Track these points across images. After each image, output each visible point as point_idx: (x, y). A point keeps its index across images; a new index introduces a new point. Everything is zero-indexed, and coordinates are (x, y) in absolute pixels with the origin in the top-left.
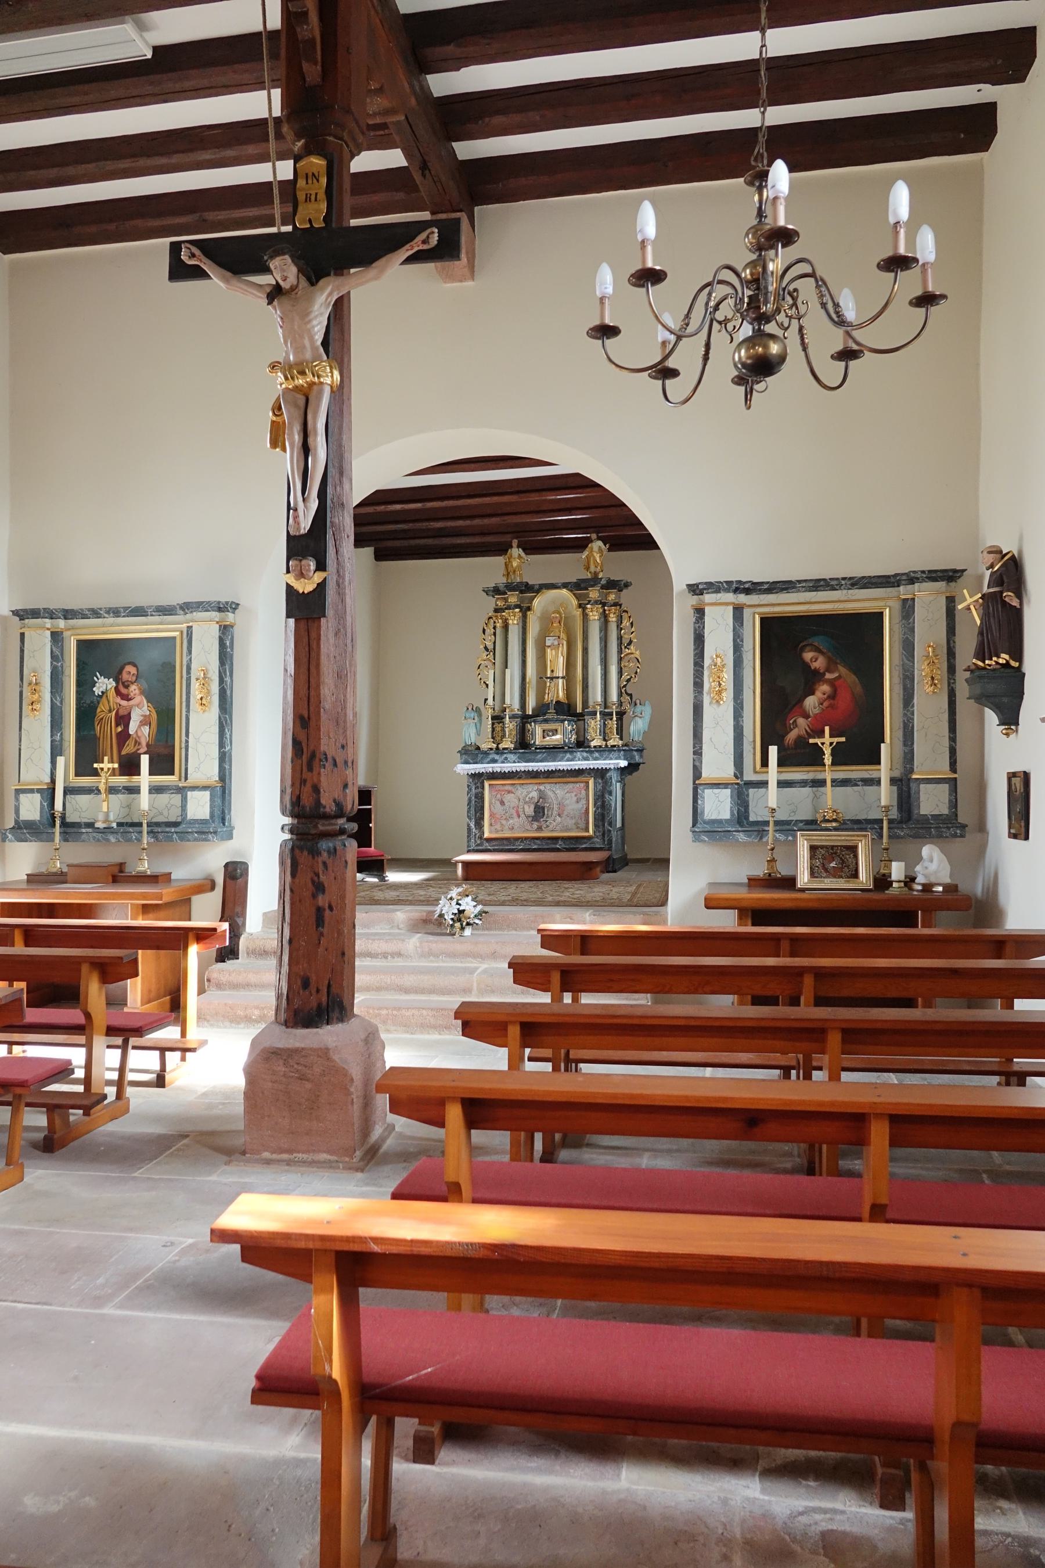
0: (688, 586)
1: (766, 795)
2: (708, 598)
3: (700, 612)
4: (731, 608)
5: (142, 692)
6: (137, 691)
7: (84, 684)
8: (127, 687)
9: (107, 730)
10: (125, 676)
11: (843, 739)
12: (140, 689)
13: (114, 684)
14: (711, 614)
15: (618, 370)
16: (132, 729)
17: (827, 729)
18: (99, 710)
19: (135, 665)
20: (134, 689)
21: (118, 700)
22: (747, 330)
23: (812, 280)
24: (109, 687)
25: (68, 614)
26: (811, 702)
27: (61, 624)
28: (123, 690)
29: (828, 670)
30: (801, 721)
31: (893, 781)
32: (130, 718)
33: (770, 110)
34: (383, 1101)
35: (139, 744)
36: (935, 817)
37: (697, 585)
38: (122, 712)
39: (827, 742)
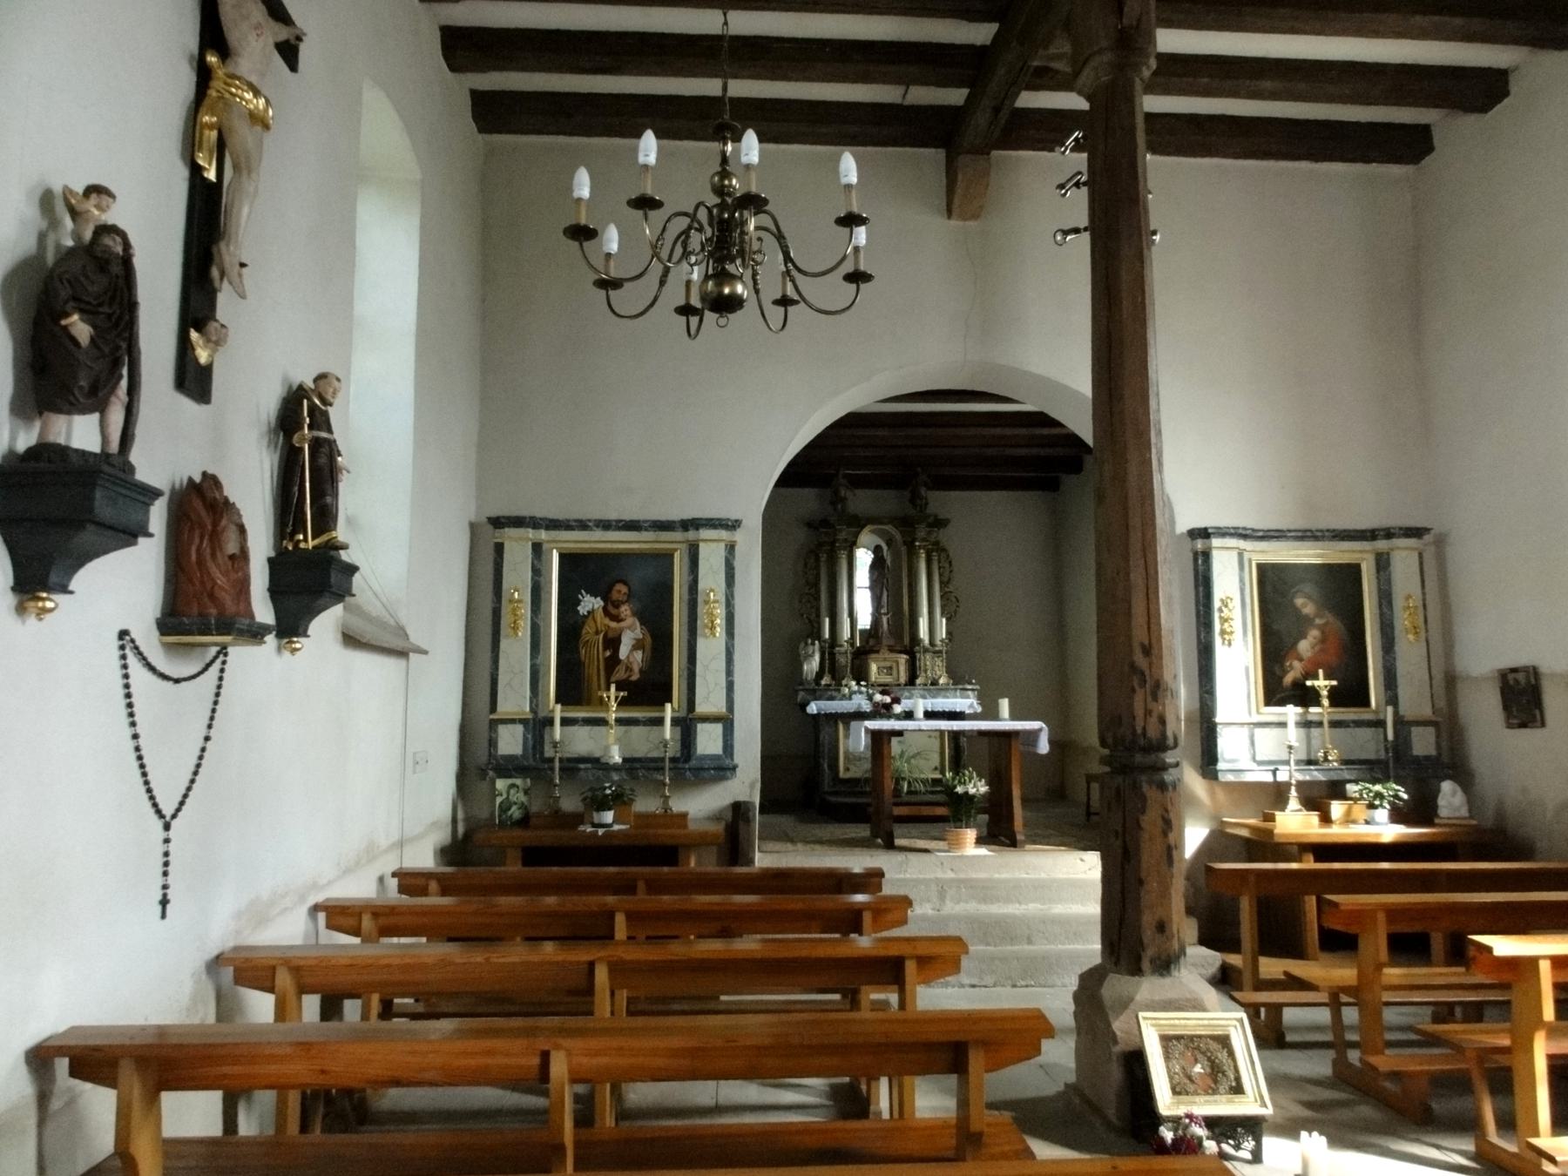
1: (663, 732)
2: (1216, 542)
3: (499, 549)
4: (722, 545)
5: (634, 614)
8: (617, 607)
9: (593, 654)
10: (615, 596)
11: (1334, 683)
14: (704, 551)
15: (837, 317)
16: (624, 652)
17: (1321, 672)
19: (625, 583)
20: (625, 610)
21: (607, 621)
25: (553, 525)
26: (1304, 647)
27: (543, 535)
28: (613, 611)
29: (1317, 615)
30: (1296, 664)
31: (675, 722)
34: (62, 1065)
36: (1427, 758)
38: (611, 635)
39: (1322, 683)
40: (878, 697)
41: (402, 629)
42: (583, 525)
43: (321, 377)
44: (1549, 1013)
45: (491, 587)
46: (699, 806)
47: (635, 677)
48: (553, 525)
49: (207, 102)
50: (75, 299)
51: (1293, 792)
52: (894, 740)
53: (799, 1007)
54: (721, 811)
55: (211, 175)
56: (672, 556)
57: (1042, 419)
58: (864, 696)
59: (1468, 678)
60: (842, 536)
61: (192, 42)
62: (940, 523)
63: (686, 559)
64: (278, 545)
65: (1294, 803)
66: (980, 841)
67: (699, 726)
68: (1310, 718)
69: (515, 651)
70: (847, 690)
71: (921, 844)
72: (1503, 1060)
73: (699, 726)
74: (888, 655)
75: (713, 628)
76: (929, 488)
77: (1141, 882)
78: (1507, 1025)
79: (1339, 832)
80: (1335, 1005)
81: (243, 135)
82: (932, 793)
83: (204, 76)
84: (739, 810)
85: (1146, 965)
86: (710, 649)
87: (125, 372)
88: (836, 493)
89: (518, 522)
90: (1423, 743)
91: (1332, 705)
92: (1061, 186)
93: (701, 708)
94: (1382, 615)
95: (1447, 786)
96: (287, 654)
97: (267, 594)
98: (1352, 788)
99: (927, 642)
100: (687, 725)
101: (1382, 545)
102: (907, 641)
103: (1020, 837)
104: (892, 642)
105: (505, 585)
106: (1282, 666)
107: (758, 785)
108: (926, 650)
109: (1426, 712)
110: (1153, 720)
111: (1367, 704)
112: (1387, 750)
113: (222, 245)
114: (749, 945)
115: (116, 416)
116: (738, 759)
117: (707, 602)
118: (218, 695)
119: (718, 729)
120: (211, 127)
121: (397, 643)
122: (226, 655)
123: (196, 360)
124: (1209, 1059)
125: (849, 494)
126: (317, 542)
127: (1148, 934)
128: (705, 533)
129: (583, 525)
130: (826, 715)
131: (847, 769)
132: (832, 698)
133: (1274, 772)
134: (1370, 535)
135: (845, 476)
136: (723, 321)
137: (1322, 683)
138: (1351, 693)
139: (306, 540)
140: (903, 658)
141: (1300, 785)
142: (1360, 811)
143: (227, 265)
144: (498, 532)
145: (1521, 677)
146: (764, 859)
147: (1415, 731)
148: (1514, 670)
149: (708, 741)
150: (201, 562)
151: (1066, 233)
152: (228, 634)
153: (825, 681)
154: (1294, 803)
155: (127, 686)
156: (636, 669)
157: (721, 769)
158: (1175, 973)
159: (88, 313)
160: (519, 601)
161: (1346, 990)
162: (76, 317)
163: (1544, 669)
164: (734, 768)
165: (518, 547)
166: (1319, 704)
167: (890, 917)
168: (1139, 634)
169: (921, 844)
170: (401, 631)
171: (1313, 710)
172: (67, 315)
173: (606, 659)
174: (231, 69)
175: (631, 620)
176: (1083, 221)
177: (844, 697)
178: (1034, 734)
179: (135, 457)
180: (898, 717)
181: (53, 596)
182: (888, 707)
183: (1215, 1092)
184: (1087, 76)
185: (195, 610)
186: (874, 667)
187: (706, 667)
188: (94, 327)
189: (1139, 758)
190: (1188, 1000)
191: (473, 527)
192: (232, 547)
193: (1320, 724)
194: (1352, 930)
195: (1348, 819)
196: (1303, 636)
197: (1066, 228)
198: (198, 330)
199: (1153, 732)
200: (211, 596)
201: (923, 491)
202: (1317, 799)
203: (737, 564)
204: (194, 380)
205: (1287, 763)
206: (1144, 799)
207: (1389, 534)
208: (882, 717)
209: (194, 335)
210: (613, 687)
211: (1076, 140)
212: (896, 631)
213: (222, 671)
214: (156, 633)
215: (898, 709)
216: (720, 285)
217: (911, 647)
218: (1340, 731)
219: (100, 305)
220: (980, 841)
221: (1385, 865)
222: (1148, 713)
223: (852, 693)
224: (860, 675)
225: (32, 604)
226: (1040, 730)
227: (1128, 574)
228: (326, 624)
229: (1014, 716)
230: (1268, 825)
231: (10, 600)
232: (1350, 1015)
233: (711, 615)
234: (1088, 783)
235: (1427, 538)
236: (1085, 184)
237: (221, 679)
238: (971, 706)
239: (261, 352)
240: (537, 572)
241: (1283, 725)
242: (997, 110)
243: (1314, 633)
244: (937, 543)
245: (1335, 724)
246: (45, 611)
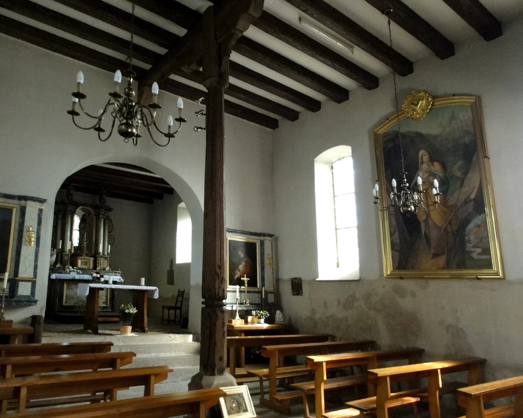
1: (3, 285)
30: (238, 273)
31: (9, 280)
39: (245, 279)
40: (95, 275)
44: (325, 378)
46: (17, 316)
51: (237, 314)
52: (100, 291)
53: (77, 400)
54: (27, 319)
57: (161, 181)
58: (76, 273)
59: (283, 280)
60: (70, 208)
62: (109, 209)
65: (238, 317)
66: (133, 331)
67: (20, 283)
68: (242, 290)
70: (68, 270)
71: (107, 332)
72: (312, 392)
73: (20, 283)
74: (86, 257)
76: (107, 196)
77: (215, 344)
78: (314, 382)
79: (249, 326)
80: (261, 381)
82: (103, 312)
84: (35, 319)
85: (216, 372)
86: (27, 252)
88: (68, 191)
90: (271, 299)
91: (248, 286)
92: (197, 113)
93: (22, 274)
94: (261, 259)
95: (278, 312)
98: (254, 313)
99: (101, 254)
100: (14, 283)
101: (262, 238)
102: (93, 252)
103: (146, 329)
104: (87, 252)
106: (234, 272)
107: (45, 309)
108: (101, 257)
109: (272, 289)
110: (221, 290)
111: (257, 286)
112: (262, 300)
114: (65, 375)
116: (36, 298)
119: (30, 284)
124: (237, 402)
125: (74, 193)
127: (217, 361)
130: (59, 279)
131: (67, 302)
132: (60, 273)
133: (232, 307)
134: (259, 235)
135: (73, 186)
136: (126, 140)
137: (245, 279)
138: (252, 283)
140: (92, 259)
141: (239, 311)
142: (256, 319)
145: (297, 281)
146: (46, 340)
147: (269, 295)
148: (295, 279)
149: (24, 289)
151: (198, 128)
153: (58, 265)
154: (238, 317)
157: (30, 301)
158: (224, 374)
161: (265, 376)
163: (303, 279)
164: (36, 301)
166: (244, 286)
167: (127, 360)
168: (218, 262)
169: (107, 332)
171: (242, 287)
176: (204, 126)
177: (66, 273)
178: (153, 292)
180: (103, 283)
182: (98, 279)
183: (239, 412)
184: (208, 82)
186: (79, 262)
189: (216, 302)
190: (229, 383)
193: (244, 292)
194: (269, 357)
195: (253, 322)
196: (241, 264)
197: (198, 126)
199: (221, 295)
201: (104, 196)
202: (244, 315)
203: (43, 217)
205: (236, 304)
206: (217, 316)
207: (264, 235)
208: (96, 282)
211: (202, 100)
212: (89, 248)
215: (102, 280)
217: (95, 255)
218: (249, 294)
220: (133, 331)
221: (263, 337)
222: (220, 287)
223: (70, 271)
224: (74, 264)
226: (156, 290)
227: (215, 242)
229: (146, 284)
230: (230, 324)
232: (266, 384)
233: (30, 237)
234: (163, 309)
235: (273, 238)
236: (205, 114)
238: (120, 279)
241: (235, 292)
242: (163, 77)
243: (243, 263)
244: (108, 217)
245: (248, 292)
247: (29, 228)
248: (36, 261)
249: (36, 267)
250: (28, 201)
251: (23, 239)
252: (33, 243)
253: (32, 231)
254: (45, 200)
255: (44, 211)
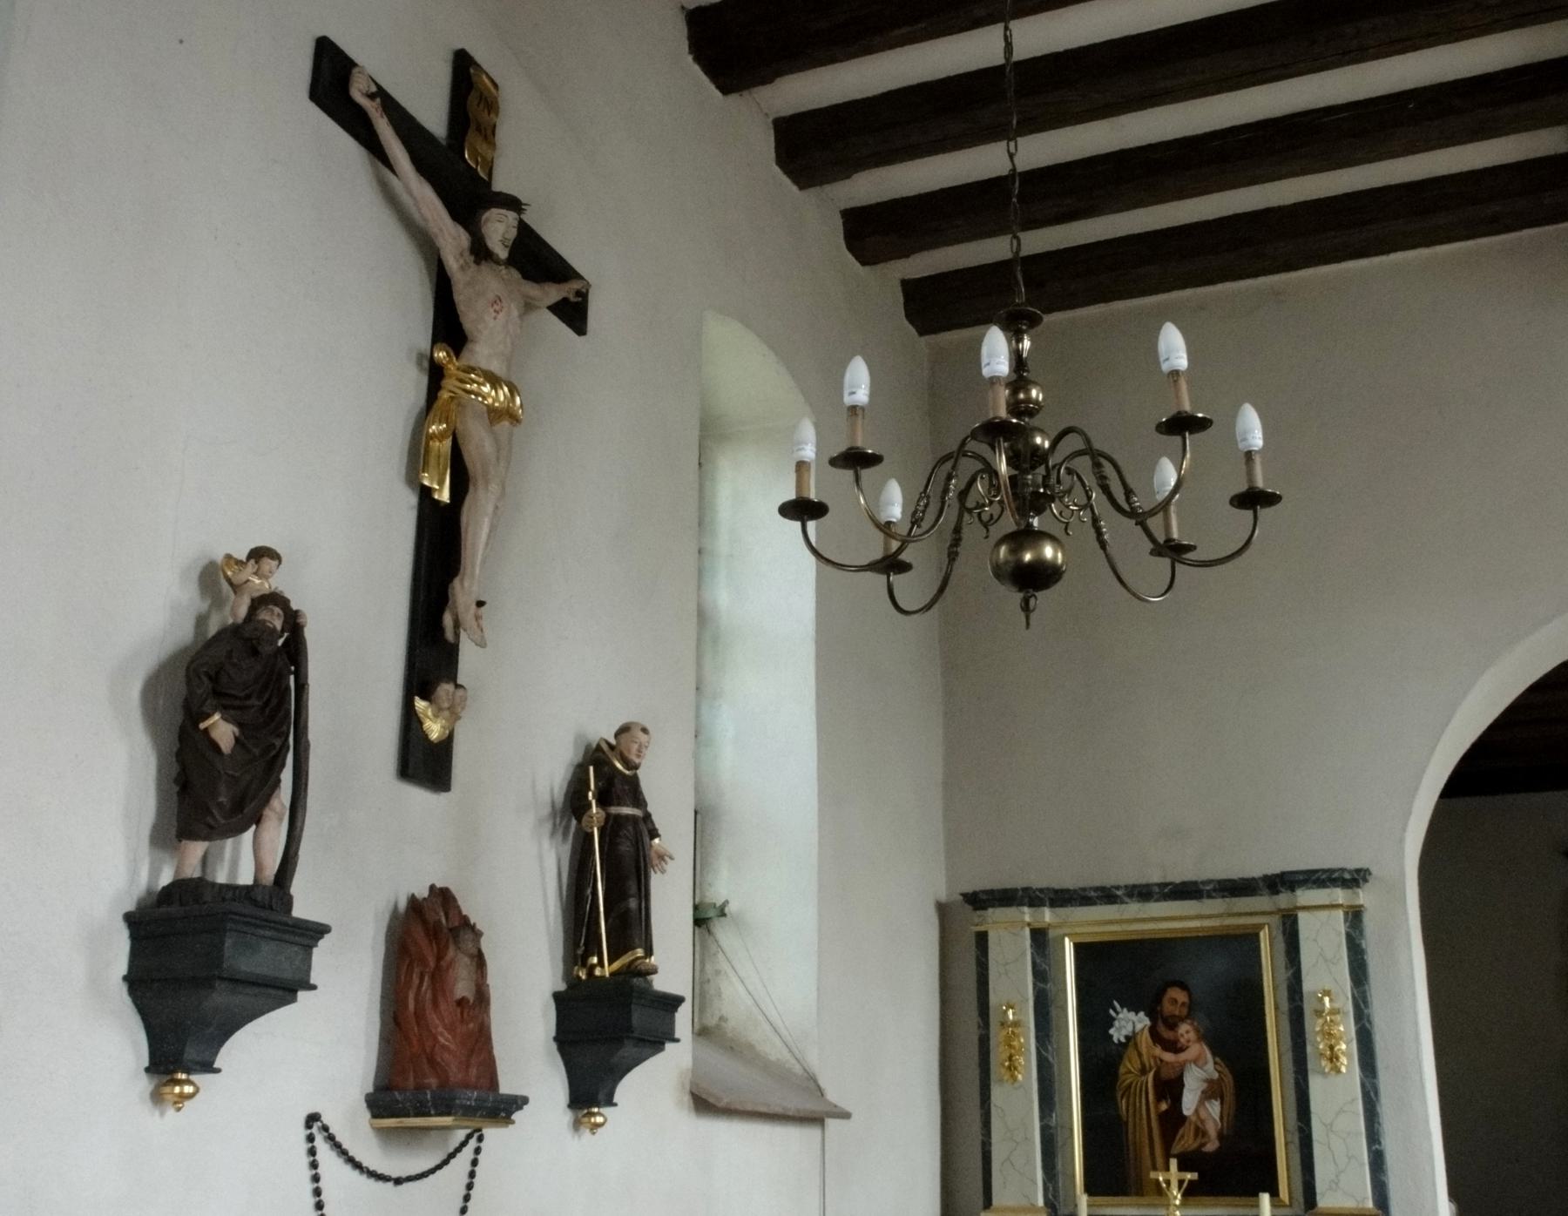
0: (964, 895)
3: (982, 939)
4: (1340, 914)
5: (1203, 1037)
6: (1192, 1035)
7: (1094, 1023)
8: (1173, 1026)
10: (1167, 1008)
12: (1197, 1031)
13: (1147, 1022)
14: (1307, 924)
18: (1122, 1070)
19: (1183, 986)
20: (1185, 1031)
21: (1158, 1051)
22: (1009, 524)
23: (1087, 458)
24: (1139, 1027)
25: (1061, 898)
27: (1047, 915)
28: (1167, 1034)
32: (1183, 1085)
33: (1024, 236)
35: (1205, 1134)
37: (975, 894)
38: (1167, 1074)
41: (813, 1079)
42: (1107, 896)
43: (624, 730)
45: (975, 1003)
47: (1212, 1146)
48: (1061, 898)
49: (438, 404)
50: (217, 694)
55: (444, 496)
56: (1257, 935)
61: (423, 339)
63: (1281, 946)
64: (569, 976)
69: (1016, 1103)
75: (1333, 1058)
81: (480, 443)
83: (436, 374)
86: (1335, 1096)
87: (287, 776)
89: (1006, 898)
96: (587, 1133)
97: (554, 1046)
105: (993, 999)
113: (456, 582)
115: (275, 832)
117: (1319, 1013)
118: (467, 1198)
120: (441, 436)
121: (794, 1103)
122: (480, 1139)
123: (425, 736)
126: (617, 965)
128: (1306, 896)
129: (1107, 896)
139: (601, 963)
143: (461, 609)
144: (976, 916)
150: (419, 1015)
152: (449, 1114)
155: (317, 1192)
156: (1212, 1131)
159: (231, 710)
160: (1016, 1024)
162: (217, 717)
165: (1009, 938)
170: (812, 1085)
172: (208, 716)
173: (1163, 1117)
174: (467, 359)
175: (1197, 1049)
179: (297, 887)
181: (193, 1077)
185: (411, 1083)
187: (1329, 1127)
188: (240, 725)
191: (943, 910)
192: (463, 988)
198: (425, 697)
200: (432, 1062)
204: (425, 763)
209: (420, 704)
210: (1174, 1163)
213: (475, 1163)
214: (366, 1115)
216: (1016, 550)
219: (248, 697)
225: (167, 1089)
228: (652, 1086)
231: (145, 1084)
237: (472, 1175)
239: (532, 709)
240: (1040, 975)
246: (184, 1097)
247: (1321, 1000)
248: (1373, 1136)
249: (1377, 1162)
250: (1299, 892)
251: (1309, 1049)
252: (1344, 1060)
253: (1334, 1012)
254: (1358, 871)
255: (1368, 921)
